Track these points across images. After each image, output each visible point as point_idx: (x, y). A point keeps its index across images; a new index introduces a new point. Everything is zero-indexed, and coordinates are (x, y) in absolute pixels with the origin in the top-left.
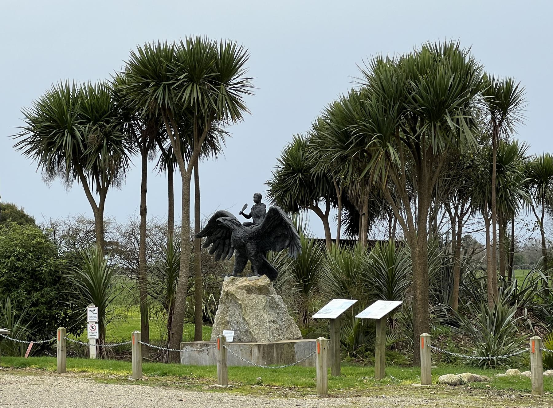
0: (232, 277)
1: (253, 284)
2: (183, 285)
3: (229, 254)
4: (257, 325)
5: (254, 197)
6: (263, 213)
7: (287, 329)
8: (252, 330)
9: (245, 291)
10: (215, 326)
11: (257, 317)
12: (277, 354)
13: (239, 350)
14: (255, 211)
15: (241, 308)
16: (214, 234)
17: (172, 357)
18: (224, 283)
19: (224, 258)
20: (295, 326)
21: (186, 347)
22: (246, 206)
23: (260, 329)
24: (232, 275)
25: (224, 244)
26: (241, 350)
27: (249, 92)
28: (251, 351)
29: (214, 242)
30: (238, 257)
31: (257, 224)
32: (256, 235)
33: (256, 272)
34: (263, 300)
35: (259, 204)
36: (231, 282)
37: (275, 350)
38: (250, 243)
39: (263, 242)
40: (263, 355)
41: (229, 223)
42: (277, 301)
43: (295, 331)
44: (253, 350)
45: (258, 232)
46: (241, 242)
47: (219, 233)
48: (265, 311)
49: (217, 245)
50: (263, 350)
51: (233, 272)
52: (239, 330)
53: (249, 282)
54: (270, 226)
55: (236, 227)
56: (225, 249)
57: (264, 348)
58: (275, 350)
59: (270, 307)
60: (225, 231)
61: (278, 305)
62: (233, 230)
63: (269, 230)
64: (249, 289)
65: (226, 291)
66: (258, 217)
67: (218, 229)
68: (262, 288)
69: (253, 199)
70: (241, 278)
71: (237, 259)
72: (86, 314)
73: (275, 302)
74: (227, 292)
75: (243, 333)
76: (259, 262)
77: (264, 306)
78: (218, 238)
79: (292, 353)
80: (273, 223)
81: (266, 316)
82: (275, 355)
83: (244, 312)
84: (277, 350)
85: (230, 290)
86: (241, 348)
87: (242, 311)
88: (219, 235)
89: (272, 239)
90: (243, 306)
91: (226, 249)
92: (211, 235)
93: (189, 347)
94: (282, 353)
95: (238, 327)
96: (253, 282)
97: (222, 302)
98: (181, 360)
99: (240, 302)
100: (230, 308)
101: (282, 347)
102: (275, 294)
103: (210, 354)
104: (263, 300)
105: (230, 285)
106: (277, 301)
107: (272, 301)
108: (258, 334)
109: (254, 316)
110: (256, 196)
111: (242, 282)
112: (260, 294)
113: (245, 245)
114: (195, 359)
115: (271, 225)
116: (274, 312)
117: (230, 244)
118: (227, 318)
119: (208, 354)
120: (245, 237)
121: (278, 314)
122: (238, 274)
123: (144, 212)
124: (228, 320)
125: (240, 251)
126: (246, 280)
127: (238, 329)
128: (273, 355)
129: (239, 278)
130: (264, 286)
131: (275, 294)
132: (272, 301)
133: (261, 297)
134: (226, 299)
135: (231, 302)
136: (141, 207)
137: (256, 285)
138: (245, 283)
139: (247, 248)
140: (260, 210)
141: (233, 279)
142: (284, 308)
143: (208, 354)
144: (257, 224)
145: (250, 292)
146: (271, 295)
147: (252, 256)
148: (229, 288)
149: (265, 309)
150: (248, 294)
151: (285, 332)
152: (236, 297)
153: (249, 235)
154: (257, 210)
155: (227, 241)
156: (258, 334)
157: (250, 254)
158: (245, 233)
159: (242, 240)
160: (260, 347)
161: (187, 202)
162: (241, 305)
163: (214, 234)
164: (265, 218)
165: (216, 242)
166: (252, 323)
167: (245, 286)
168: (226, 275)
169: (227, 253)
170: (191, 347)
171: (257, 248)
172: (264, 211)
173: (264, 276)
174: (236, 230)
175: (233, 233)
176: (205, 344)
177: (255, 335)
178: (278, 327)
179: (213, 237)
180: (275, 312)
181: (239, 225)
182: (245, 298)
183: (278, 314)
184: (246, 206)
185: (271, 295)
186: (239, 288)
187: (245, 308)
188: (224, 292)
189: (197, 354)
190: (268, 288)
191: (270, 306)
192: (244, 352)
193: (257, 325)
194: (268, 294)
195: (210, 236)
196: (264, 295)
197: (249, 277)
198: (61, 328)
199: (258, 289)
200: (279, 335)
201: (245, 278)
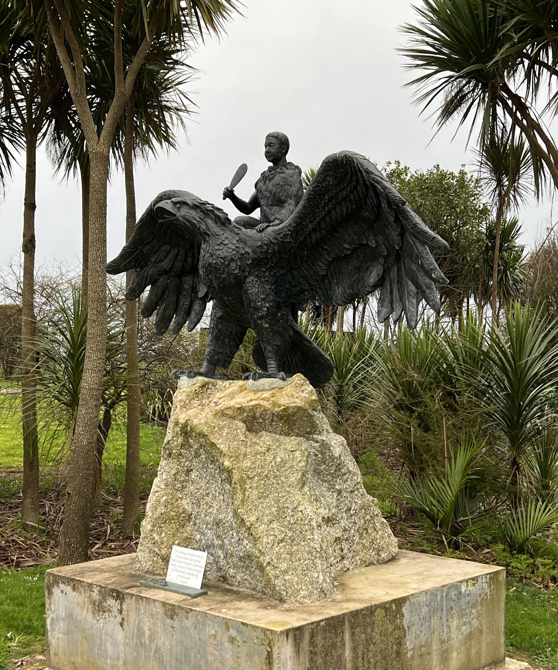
0: (200, 378)
1: (265, 403)
2: (91, 389)
3: (193, 314)
4: (282, 541)
5: (268, 145)
6: (294, 189)
7: (361, 535)
8: (267, 559)
9: (241, 425)
10: (149, 527)
11: (281, 510)
12: (354, 649)
13: (225, 638)
14: (270, 185)
15: (229, 480)
16: (153, 260)
17: (65, 543)
18: (178, 397)
19: (180, 326)
20: (382, 523)
21: (62, 586)
22: (243, 170)
23: (291, 554)
24: (201, 374)
25: (179, 290)
26: (232, 640)
27: (235, 7)
28: (269, 656)
29: (153, 283)
30: (216, 320)
31: (277, 222)
32: (274, 254)
33: (272, 365)
34: (298, 454)
35: (281, 163)
36: (197, 393)
37: (347, 636)
38: (257, 276)
39: (294, 278)
40: (311, 660)
41: (194, 215)
42: (337, 455)
43: (382, 537)
44: (275, 650)
45: (282, 244)
46: (229, 274)
47: (165, 257)
48: (306, 489)
49: (160, 292)
50: (312, 643)
51: (205, 364)
52: (222, 547)
53: (252, 396)
54: (319, 223)
55: (214, 228)
56: (181, 304)
57: (312, 636)
58: (347, 636)
59: (317, 472)
60: (182, 252)
61: (339, 467)
62: (205, 235)
63: (315, 237)
64: (254, 417)
65: (182, 421)
66: (280, 203)
67: (164, 248)
68: (294, 414)
69: (264, 150)
70: (227, 383)
71: (216, 325)
72: (24, 405)
73: (332, 458)
74: (185, 425)
75: (235, 560)
76: (281, 335)
77: (303, 475)
78: (165, 272)
79: (397, 633)
80: (329, 212)
81: (308, 509)
82: (348, 654)
83: (239, 496)
84: (353, 634)
85: (196, 422)
86: (233, 632)
87: (234, 492)
88: (165, 264)
89: (321, 267)
90: (236, 476)
91: (185, 302)
92: (146, 265)
93: (69, 589)
94: (369, 641)
95: (218, 537)
96: (266, 395)
97: (170, 455)
98: (48, 621)
99: (227, 463)
100: (193, 475)
101: (368, 620)
102: (328, 431)
103: (130, 626)
104: (298, 454)
105: (196, 403)
106: (337, 455)
107: (323, 454)
108: (285, 572)
109: (274, 509)
110: (274, 141)
111: (232, 396)
112: (287, 435)
113: (240, 282)
114: (84, 630)
115: (323, 219)
116: (329, 490)
117: (194, 290)
118: (186, 504)
119: (121, 624)
120: (242, 257)
121: (340, 492)
122: (220, 370)
123: (29, 245)
124: (189, 508)
125: (224, 301)
126: (242, 389)
127: (217, 542)
128: (340, 657)
129: (220, 382)
130: (299, 408)
131: (328, 431)
132: (323, 454)
133: (291, 442)
134: (183, 446)
135: (197, 455)
136: (24, 236)
137: (274, 404)
138: (241, 400)
139: (246, 292)
140: (286, 183)
141: (203, 386)
142: (354, 474)
143: (121, 624)
144: (277, 222)
145: (256, 426)
146: (319, 438)
147: (261, 318)
148: (191, 412)
149: (304, 484)
150: (250, 435)
151: (358, 544)
152: (213, 445)
153: (253, 252)
154: (277, 179)
155: (188, 281)
156: (285, 572)
157: (257, 309)
158: (241, 245)
159: (233, 265)
160: (302, 634)
161: (101, 208)
162: (229, 472)
163: (153, 260)
164: (300, 206)
165: (159, 284)
166: (268, 535)
167: (241, 409)
168: (182, 373)
169: (188, 313)
170: (74, 589)
171: (277, 293)
172: (298, 184)
173: (299, 378)
174: (215, 235)
175: (203, 246)
176: (113, 590)
177: (277, 577)
178: (339, 535)
179: (150, 270)
180: (331, 488)
181: (224, 221)
182: (243, 448)
183: (340, 492)
184: (243, 170)
185: (319, 438)
186: (222, 414)
187: (242, 481)
188: (177, 424)
189: (90, 617)
190: (311, 416)
191: (315, 471)
192: (244, 649)
193: (282, 541)
194: (310, 433)
195: (142, 268)
196: (298, 435)
197: (250, 381)
198: (303, 317)
199: (281, 417)
200: (343, 558)
201: (241, 382)
